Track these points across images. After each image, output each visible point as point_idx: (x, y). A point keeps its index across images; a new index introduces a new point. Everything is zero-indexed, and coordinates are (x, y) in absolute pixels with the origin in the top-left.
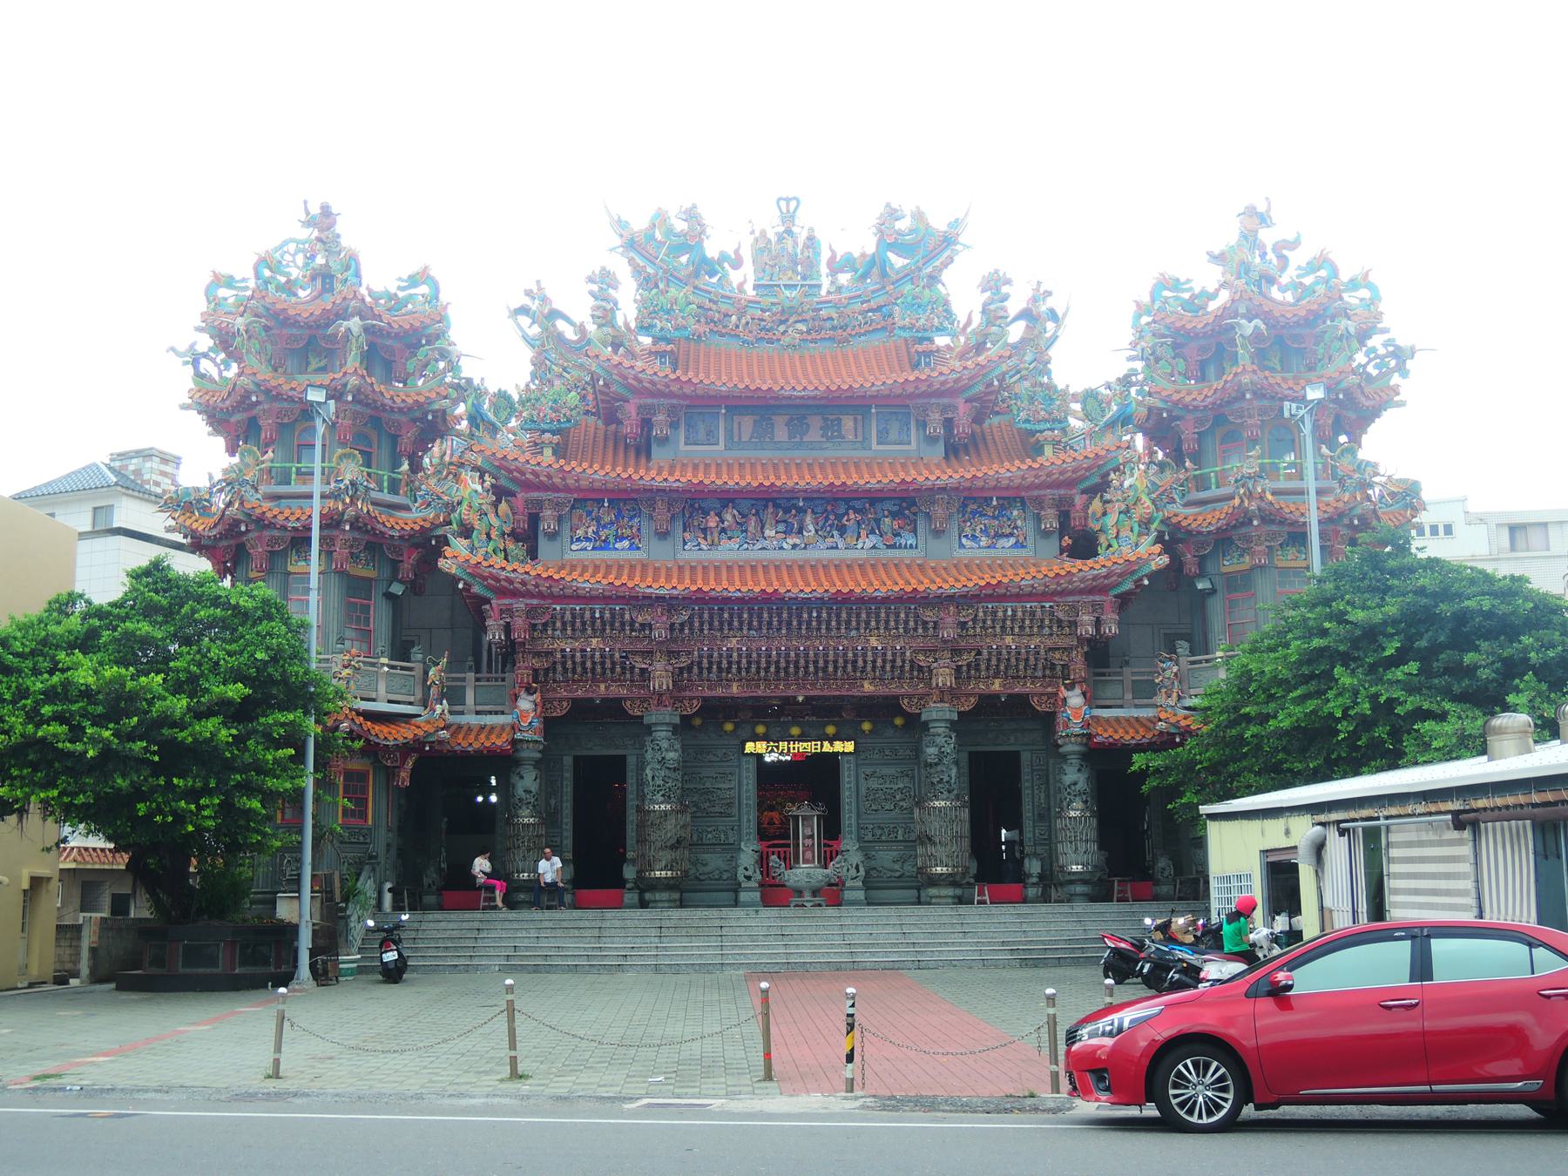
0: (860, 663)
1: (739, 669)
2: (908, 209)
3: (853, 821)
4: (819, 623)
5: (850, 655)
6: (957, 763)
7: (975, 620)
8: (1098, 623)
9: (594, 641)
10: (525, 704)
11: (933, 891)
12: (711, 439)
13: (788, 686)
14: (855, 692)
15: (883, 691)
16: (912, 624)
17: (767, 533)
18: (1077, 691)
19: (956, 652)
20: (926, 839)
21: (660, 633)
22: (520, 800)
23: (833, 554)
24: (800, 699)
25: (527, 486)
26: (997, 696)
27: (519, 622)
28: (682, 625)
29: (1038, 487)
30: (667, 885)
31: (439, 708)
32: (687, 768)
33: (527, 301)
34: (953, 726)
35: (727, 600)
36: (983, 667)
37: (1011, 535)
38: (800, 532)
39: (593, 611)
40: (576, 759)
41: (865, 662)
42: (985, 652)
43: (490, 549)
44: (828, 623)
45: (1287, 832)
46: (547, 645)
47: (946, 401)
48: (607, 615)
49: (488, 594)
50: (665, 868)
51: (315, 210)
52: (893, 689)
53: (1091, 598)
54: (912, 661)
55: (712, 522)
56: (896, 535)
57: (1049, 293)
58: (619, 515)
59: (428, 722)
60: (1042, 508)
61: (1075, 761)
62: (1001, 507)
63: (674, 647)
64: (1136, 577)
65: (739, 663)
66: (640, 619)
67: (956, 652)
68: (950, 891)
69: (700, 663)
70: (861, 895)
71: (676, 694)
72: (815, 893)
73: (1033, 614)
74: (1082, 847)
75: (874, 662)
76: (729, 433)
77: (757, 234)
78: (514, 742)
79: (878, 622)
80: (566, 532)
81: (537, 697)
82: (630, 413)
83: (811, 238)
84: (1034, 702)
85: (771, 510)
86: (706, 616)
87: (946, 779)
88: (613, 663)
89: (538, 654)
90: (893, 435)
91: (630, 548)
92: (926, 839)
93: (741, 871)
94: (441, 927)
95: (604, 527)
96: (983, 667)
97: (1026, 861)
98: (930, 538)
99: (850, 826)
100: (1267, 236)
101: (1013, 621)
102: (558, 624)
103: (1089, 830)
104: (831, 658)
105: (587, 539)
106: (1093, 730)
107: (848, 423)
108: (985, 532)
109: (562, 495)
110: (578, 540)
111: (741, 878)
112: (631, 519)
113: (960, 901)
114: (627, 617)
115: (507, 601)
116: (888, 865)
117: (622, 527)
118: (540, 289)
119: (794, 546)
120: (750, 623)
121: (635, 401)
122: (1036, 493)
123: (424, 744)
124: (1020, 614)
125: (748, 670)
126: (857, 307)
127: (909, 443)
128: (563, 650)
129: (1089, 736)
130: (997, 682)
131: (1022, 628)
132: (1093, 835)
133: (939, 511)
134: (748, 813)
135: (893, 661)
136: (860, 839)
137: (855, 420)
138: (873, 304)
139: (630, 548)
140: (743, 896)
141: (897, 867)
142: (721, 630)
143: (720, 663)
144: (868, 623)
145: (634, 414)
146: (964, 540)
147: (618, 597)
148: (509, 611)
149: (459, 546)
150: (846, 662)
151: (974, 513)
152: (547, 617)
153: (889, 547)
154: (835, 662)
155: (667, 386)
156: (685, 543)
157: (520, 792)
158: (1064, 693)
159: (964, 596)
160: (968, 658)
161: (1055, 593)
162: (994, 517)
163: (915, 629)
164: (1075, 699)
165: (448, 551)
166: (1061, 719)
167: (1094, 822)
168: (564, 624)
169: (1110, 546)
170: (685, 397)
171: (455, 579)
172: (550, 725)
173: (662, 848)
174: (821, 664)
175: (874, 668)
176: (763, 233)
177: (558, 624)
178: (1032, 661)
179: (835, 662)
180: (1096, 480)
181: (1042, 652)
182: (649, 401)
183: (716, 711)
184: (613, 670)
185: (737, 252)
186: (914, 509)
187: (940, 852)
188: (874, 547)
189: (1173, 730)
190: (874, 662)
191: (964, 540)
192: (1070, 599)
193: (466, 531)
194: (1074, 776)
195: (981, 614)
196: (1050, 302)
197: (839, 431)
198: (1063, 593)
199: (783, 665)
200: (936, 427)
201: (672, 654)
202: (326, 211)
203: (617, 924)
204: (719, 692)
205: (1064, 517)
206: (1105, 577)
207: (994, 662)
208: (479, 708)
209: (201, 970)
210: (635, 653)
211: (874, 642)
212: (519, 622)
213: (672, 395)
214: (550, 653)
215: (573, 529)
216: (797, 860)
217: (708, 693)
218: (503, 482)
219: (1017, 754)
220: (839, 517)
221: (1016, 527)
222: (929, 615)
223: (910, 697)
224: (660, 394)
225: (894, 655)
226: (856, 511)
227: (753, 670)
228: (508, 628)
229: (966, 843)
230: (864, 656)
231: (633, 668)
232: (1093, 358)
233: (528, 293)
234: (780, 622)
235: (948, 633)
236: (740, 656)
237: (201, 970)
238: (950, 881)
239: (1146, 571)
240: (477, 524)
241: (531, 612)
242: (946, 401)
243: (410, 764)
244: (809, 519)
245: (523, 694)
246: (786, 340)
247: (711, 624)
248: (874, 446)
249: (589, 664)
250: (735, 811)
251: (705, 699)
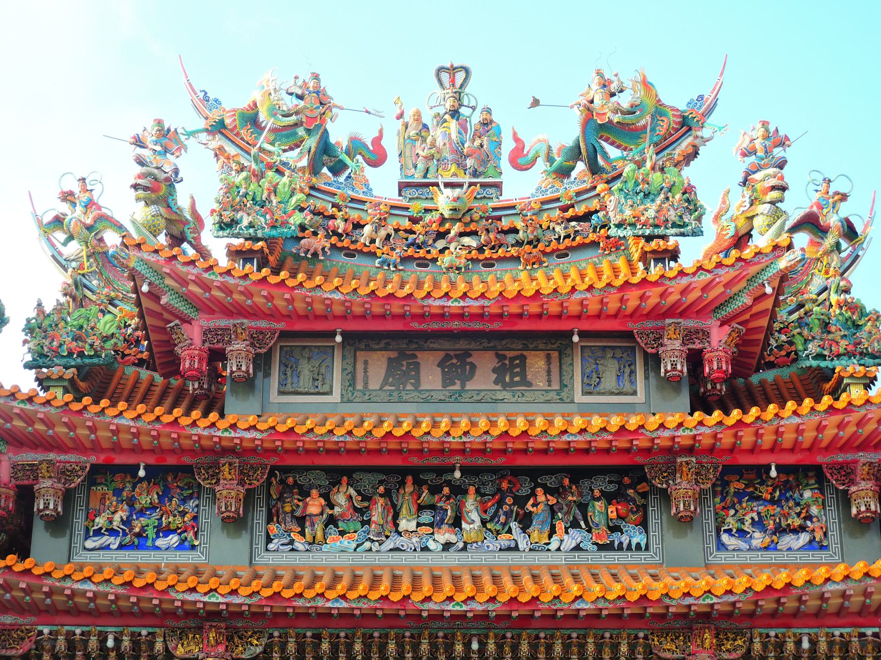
2: (628, 77)
17: (404, 524)
29: (848, 446)
35: (326, 616)
37: (802, 529)
38: (457, 523)
39: (103, 639)
47: (691, 323)
48: (126, 643)
55: (314, 505)
56: (615, 529)
57: (844, 197)
60: (853, 482)
62: (786, 487)
76: (351, 381)
77: (408, 117)
80: (79, 521)
82: (191, 343)
83: (487, 124)
85: (409, 488)
90: (609, 381)
91: (181, 546)
95: (142, 513)
105: (112, 532)
107: (536, 364)
108: (759, 524)
109: (72, 457)
110: (98, 533)
112: (184, 501)
114: (159, 646)
117: (169, 513)
118: (85, 190)
119: (447, 546)
122: (840, 458)
127: (634, 393)
133: (683, 488)
137: (548, 358)
138: (581, 209)
139: (181, 546)
146: (725, 538)
147: (144, 614)
151: (739, 495)
153: (601, 548)
156: (269, 540)
159: (728, 616)
162: (772, 502)
170: (274, 315)
176: (418, 117)
182: (223, 323)
185: (377, 141)
186: (643, 487)
188: (577, 548)
191: (725, 538)
196: (845, 210)
197: (523, 374)
200: (673, 360)
215: (91, 517)
220: (520, 501)
221: (809, 517)
226: (548, 491)
233: (67, 197)
242: (691, 323)
244: (471, 504)
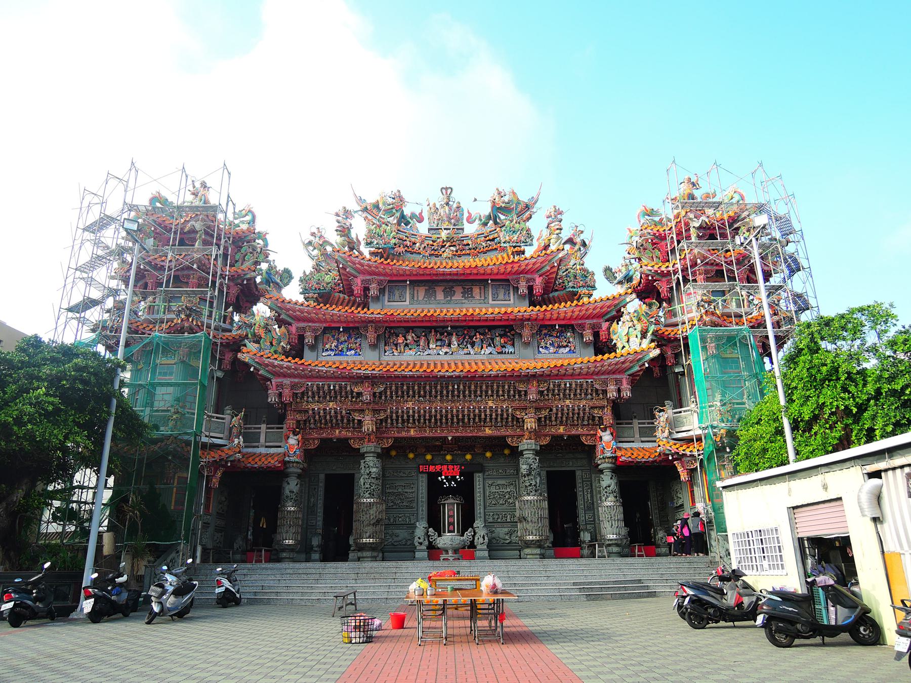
0: (483, 416)
1: (414, 420)
3: (482, 511)
4: (459, 392)
5: (477, 411)
6: (539, 474)
7: (548, 390)
8: (619, 391)
9: (331, 404)
10: (292, 441)
11: (527, 551)
13: (442, 431)
14: (480, 434)
15: (496, 433)
16: (512, 392)
17: (431, 346)
18: (608, 432)
19: (538, 409)
20: (523, 519)
21: (367, 397)
22: (287, 497)
23: (468, 357)
24: (450, 438)
25: (298, 319)
26: (561, 436)
27: (287, 392)
28: (380, 393)
29: (582, 318)
30: (371, 547)
31: (236, 441)
32: (383, 476)
33: (312, 238)
35: (405, 377)
36: (553, 419)
37: (567, 346)
38: (449, 345)
40: (327, 476)
41: (486, 415)
42: (554, 409)
43: (272, 351)
44: (464, 392)
45: (825, 487)
46: (304, 406)
47: (529, 276)
48: (337, 387)
49: (269, 376)
50: (370, 537)
52: (503, 432)
53: (615, 376)
54: (512, 415)
57: (582, 232)
58: (350, 337)
59: (229, 449)
62: (562, 332)
63: (376, 407)
64: (640, 363)
65: (413, 416)
66: (356, 390)
67: (538, 409)
68: (538, 551)
69: (391, 417)
70: (486, 554)
71: (378, 435)
72: (456, 551)
73: (581, 385)
74: (615, 524)
75: (491, 415)
78: (285, 463)
79: (492, 392)
80: (320, 346)
81: (299, 437)
83: (458, 207)
84: (583, 439)
86: (393, 388)
87: (533, 483)
88: (342, 417)
89: (300, 412)
91: (355, 354)
92: (523, 519)
93: (416, 539)
94: (259, 576)
95: (341, 343)
96: (553, 419)
97: (582, 533)
98: (522, 349)
99: (480, 513)
101: (570, 390)
102: (310, 393)
103: (619, 513)
104: (466, 413)
105: (332, 350)
106: (619, 454)
107: (476, 291)
108: (552, 344)
109: (317, 325)
110: (327, 350)
111: (417, 544)
113: (543, 556)
114: (348, 388)
115: (280, 380)
116: (502, 536)
119: (446, 353)
120: (419, 393)
121: (361, 277)
123: (227, 462)
124: (574, 386)
125: (419, 420)
128: (313, 409)
129: (616, 458)
130: (562, 428)
131: (575, 395)
132: (621, 516)
133: (526, 332)
134: (422, 506)
135: (502, 415)
136: (485, 521)
139: (355, 354)
140: (418, 555)
141: (507, 537)
142: (403, 397)
143: (402, 417)
144: (487, 392)
145: (360, 284)
148: (280, 386)
149: (252, 346)
150: (475, 416)
152: (303, 389)
153: (499, 353)
154: (469, 415)
155: (377, 267)
157: (287, 492)
158: (602, 434)
160: (544, 413)
161: (594, 373)
162: (557, 337)
163: (514, 396)
164: (607, 437)
165: (244, 349)
166: (599, 448)
167: (621, 509)
168: (313, 393)
169: (624, 347)
171: (248, 366)
172: (309, 455)
173: (367, 525)
174: (460, 417)
175: (491, 419)
177: (310, 393)
178: (581, 414)
179: (469, 415)
180: (614, 313)
181: (587, 409)
183: (402, 446)
184: (342, 421)
185: (421, 214)
186: (513, 332)
187: (529, 526)
188: (491, 353)
189: (667, 452)
190: (491, 415)
192: (603, 377)
193: (257, 340)
194: (607, 481)
195: (552, 386)
196: (582, 237)
198: (598, 374)
199: (438, 417)
200: (523, 289)
201: (375, 411)
203: (333, 571)
204: (404, 434)
205: (596, 335)
206: (623, 363)
207: (560, 415)
208: (268, 444)
210: (354, 411)
211: (490, 404)
212: (287, 392)
213: (379, 274)
214: (306, 411)
215: (324, 345)
216: (444, 532)
217: (397, 435)
218: (283, 316)
219: (573, 472)
220: (471, 338)
222: (522, 387)
223: (513, 437)
224: (374, 273)
225: (502, 411)
226: (480, 334)
227: (422, 421)
228: (280, 395)
229: (547, 522)
230: (485, 411)
231: (354, 420)
232: (607, 258)
233: (313, 234)
234: (436, 392)
235: (532, 396)
236: (414, 412)
238: (538, 544)
239: (647, 358)
240: (263, 335)
241: (293, 386)
242: (529, 276)
243: (219, 474)
244: (454, 338)
245: (291, 435)
247: (397, 393)
248: (491, 302)
249: (328, 417)
250: (414, 505)
251: (396, 439)
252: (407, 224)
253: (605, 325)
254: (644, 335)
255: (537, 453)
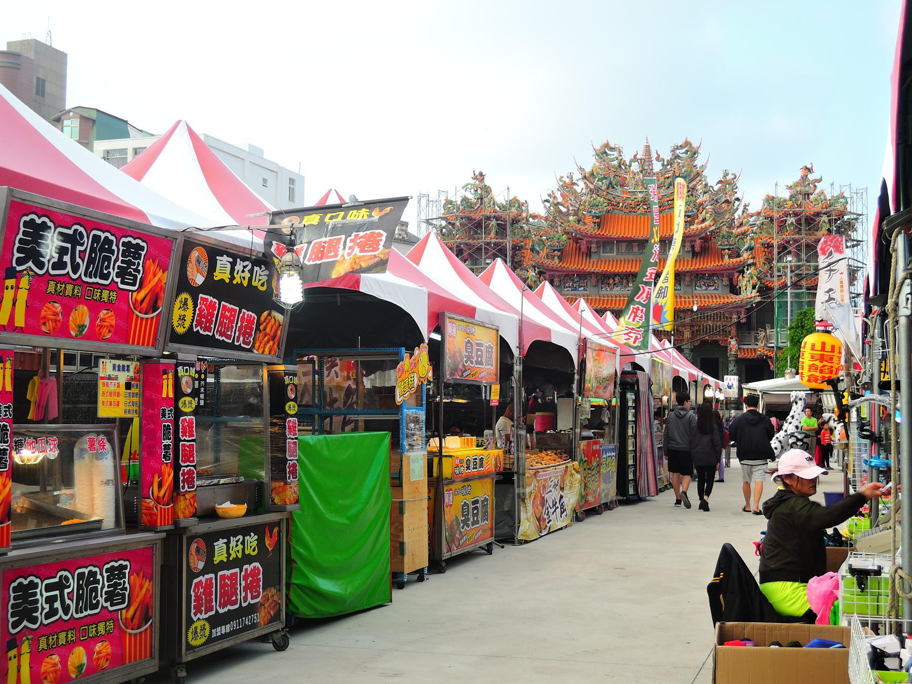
12: (611, 251)
19: (692, 326)
25: (550, 270)
34: (692, 350)
51: (477, 173)
61: (733, 363)
67: (692, 326)
100: (811, 177)
108: (704, 284)
126: (666, 199)
164: (733, 342)
202: (481, 174)
209: (315, 498)
233: (549, 195)
237: (315, 498)
246: (639, 212)
252: (613, 188)
253: (736, 274)
254: (754, 287)
255: (692, 350)
